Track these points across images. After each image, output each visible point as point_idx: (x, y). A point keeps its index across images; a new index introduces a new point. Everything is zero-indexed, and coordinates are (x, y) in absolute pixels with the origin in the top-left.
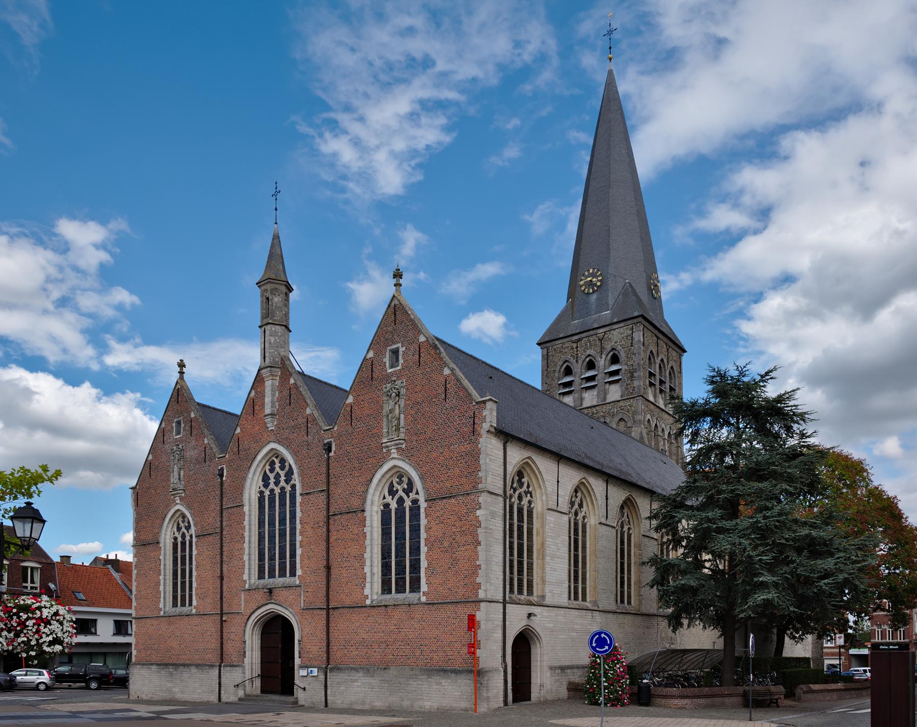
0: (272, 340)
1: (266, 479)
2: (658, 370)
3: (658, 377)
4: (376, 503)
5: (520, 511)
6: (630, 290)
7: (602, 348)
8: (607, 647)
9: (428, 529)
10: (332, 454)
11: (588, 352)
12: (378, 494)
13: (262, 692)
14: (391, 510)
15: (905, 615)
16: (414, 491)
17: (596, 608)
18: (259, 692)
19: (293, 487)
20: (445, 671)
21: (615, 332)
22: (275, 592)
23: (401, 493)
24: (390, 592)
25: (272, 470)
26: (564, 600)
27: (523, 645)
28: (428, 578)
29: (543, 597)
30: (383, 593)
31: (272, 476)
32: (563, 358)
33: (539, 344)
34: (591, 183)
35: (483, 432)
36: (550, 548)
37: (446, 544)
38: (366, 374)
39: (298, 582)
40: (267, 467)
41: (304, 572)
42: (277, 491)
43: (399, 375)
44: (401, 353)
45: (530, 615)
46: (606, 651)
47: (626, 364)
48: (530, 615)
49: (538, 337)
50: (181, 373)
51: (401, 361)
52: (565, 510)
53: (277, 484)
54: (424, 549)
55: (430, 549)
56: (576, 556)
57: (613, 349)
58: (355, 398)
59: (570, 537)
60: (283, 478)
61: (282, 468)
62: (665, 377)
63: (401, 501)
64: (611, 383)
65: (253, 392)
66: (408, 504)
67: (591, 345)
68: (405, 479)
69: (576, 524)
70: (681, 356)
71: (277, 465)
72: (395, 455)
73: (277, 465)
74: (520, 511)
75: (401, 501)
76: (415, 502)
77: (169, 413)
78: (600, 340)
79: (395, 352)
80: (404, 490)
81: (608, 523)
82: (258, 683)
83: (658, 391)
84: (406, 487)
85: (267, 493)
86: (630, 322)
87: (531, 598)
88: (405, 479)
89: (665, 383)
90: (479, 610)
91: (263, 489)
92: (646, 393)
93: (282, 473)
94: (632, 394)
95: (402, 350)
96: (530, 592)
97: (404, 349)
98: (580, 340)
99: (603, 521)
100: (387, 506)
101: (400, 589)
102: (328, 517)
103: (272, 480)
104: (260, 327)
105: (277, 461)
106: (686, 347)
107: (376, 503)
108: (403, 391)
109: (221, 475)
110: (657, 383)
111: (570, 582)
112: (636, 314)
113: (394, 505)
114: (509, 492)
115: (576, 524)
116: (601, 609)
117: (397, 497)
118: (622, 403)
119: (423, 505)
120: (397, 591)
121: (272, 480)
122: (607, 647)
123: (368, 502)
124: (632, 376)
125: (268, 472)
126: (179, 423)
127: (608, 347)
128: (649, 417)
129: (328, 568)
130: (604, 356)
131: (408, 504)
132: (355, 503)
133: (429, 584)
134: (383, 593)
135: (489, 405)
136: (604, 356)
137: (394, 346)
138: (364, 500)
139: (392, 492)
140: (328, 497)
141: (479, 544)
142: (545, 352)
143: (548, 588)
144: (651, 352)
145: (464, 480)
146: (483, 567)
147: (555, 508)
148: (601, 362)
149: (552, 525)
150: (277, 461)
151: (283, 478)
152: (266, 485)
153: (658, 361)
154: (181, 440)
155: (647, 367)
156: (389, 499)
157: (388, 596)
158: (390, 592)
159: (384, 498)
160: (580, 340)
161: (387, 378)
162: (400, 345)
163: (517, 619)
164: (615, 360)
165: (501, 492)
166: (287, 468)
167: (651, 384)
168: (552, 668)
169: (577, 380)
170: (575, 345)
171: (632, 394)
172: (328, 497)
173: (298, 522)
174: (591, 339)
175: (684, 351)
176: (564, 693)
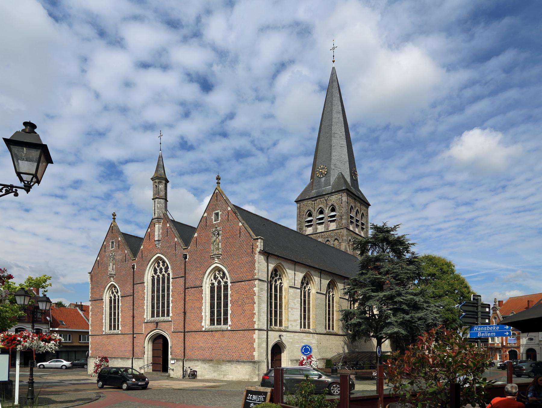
0: (159, 205)
3: (355, 218)
4: (208, 283)
7: (327, 204)
9: (231, 296)
10: (187, 260)
11: (320, 206)
12: (208, 279)
13: (153, 370)
18: (151, 371)
20: (238, 361)
21: (333, 197)
22: (159, 324)
23: (219, 278)
24: (214, 325)
25: (158, 266)
26: (298, 328)
32: (308, 208)
37: (240, 303)
38: (203, 223)
39: (170, 319)
40: (156, 265)
41: (173, 315)
42: (161, 276)
43: (219, 225)
47: (339, 212)
50: (114, 219)
51: (220, 218)
57: (332, 205)
59: (301, 299)
60: (164, 270)
61: (163, 265)
63: (219, 282)
64: (331, 221)
66: (223, 284)
69: (305, 293)
70: (367, 208)
71: (161, 264)
72: (217, 262)
73: (161, 264)
75: (219, 282)
77: (107, 238)
79: (217, 214)
82: (151, 368)
87: (281, 328)
90: (254, 333)
91: (154, 275)
95: (220, 213)
101: (219, 323)
102: (185, 289)
103: (158, 271)
104: (153, 199)
107: (208, 283)
108: (220, 232)
109: (134, 268)
112: (344, 188)
113: (216, 284)
118: (336, 231)
120: (218, 324)
121: (158, 271)
123: (204, 283)
124: (342, 218)
126: (113, 242)
127: (330, 204)
129: (185, 313)
130: (328, 208)
131: (223, 284)
132: (198, 283)
133: (232, 321)
135: (259, 240)
136: (328, 208)
138: (202, 281)
139: (215, 278)
140: (185, 280)
141: (255, 303)
145: (248, 274)
146: (257, 314)
148: (327, 211)
151: (164, 270)
154: (114, 251)
156: (214, 281)
157: (213, 327)
158: (214, 325)
160: (316, 200)
161: (213, 226)
163: (274, 338)
164: (333, 210)
168: (291, 361)
169: (314, 219)
172: (185, 280)
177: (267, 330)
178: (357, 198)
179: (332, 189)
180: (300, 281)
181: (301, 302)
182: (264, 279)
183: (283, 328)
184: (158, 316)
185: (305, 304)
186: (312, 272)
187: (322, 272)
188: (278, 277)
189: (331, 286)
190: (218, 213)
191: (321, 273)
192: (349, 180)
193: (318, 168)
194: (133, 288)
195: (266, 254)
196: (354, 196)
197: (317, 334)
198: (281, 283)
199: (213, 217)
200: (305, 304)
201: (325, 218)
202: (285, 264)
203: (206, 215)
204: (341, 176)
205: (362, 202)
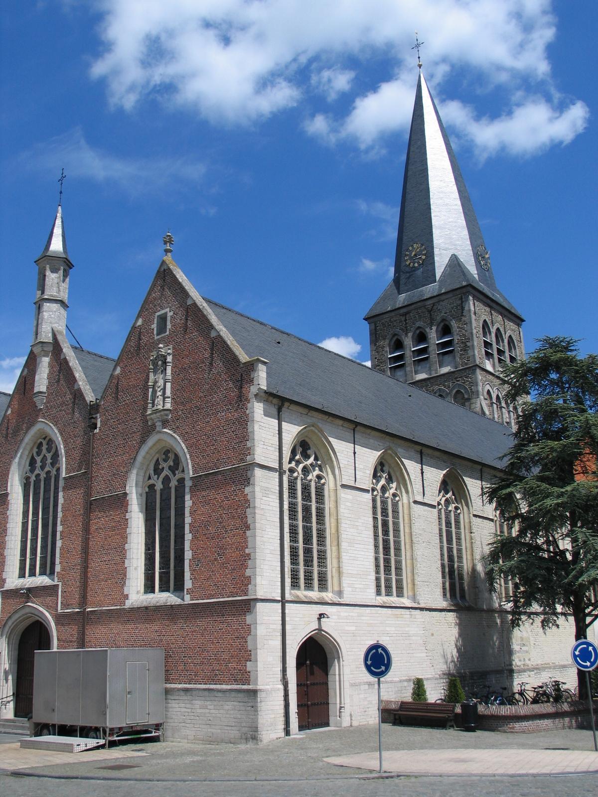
1: (32, 462)
2: (494, 339)
3: (495, 346)
5: (306, 488)
6: (455, 259)
8: (588, 664)
14: (156, 491)
15: (511, 552)
16: (180, 469)
17: (416, 605)
19: (58, 470)
24: (153, 591)
25: (38, 454)
26: (369, 595)
27: (316, 656)
28: (192, 571)
29: (340, 593)
30: (146, 592)
31: (38, 459)
33: (365, 319)
34: (410, 167)
35: (251, 396)
36: (348, 532)
40: (35, 450)
42: (43, 475)
44: (169, 318)
45: (321, 616)
46: (586, 667)
48: (321, 616)
49: (364, 314)
51: (169, 326)
52: (368, 485)
53: (42, 468)
54: (188, 536)
55: (195, 538)
56: (386, 542)
58: (123, 371)
59: (375, 519)
61: (49, 450)
62: (504, 346)
63: (167, 480)
65: (26, 370)
66: (173, 483)
67: (420, 317)
68: (171, 455)
69: (384, 503)
71: (44, 447)
73: (44, 447)
74: (306, 488)
75: (167, 480)
76: (181, 481)
78: (430, 312)
79: (163, 319)
80: (170, 468)
81: (426, 501)
83: (496, 361)
84: (172, 464)
85: (33, 478)
86: (458, 292)
87: (324, 594)
88: (171, 455)
89: (504, 352)
92: (485, 364)
93: (49, 456)
94: (466, 364)
95: (170, 314)
96: (323, 584)
97: (171, 313)
98: (408, 313)
99: (419, 498)
100: (151, 487)
103: (39, 464)
105: (44, 443)
106: (523, 317)
110: (495, 353)
111: (377, 572)
113: (159, 486)
114: (286, 466)
115: (384, 503)
116: (422, 606)
117: (163, 475)
119: (188, 483)
121: (39, 464)
122: (588, 664)
125: (35, 454)
127: (439, 318)
128: (488, 387)
131: (173, 483)
133: (194, 579)
134: (146, 592)
137: (163, 312)
142: (373, 327)
143: (345, 582)
144: (485, 321)
147: (352, 484)
149: (349, 504)
150: (44, 443)
152: (32, 470)
153: (493, 331)
155: (482, 336)
157: (151, 596)
158: (153, 591)
159: (149, 478)
160: (408, 313)
162: (168, 310)
163: (302, 624)
165: (276, 466)
166: (53, 450)
167: (487, 354)
170: (403, 319)
171: (466, 364)
173: (60, 509)
174: (420, 311)
175: (523, 321)
176: (373, 717)
177: (283, 602)
178: (494, 305)
179: (440, 287)
180: (371, 472)
181: (375, 527)
182: (566, 663)
183: (328, 596)
184: (33, 574)
185: (386, 532)
186: (400, 451)
187: (426, 453)
188: (312, 460)
189: (452, 485)
190: (166, 313)
191: (421, 453)
192: (472, 270)
193: (407, 250)
194: (86, 529)
195: (275, 401)
196: (489, 302)
197: (421, 609)
198: (319, 477)
199: (154, 326)
200: (386, 532)
201: (431, 349)
202: (326, 427)
203: (140, 322)
204: (456, 262)
205: (506, 313)
